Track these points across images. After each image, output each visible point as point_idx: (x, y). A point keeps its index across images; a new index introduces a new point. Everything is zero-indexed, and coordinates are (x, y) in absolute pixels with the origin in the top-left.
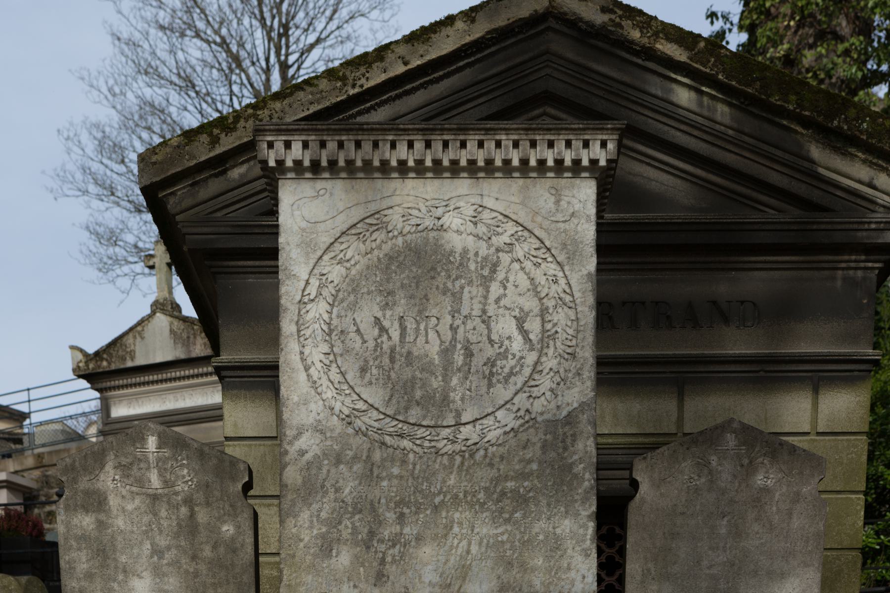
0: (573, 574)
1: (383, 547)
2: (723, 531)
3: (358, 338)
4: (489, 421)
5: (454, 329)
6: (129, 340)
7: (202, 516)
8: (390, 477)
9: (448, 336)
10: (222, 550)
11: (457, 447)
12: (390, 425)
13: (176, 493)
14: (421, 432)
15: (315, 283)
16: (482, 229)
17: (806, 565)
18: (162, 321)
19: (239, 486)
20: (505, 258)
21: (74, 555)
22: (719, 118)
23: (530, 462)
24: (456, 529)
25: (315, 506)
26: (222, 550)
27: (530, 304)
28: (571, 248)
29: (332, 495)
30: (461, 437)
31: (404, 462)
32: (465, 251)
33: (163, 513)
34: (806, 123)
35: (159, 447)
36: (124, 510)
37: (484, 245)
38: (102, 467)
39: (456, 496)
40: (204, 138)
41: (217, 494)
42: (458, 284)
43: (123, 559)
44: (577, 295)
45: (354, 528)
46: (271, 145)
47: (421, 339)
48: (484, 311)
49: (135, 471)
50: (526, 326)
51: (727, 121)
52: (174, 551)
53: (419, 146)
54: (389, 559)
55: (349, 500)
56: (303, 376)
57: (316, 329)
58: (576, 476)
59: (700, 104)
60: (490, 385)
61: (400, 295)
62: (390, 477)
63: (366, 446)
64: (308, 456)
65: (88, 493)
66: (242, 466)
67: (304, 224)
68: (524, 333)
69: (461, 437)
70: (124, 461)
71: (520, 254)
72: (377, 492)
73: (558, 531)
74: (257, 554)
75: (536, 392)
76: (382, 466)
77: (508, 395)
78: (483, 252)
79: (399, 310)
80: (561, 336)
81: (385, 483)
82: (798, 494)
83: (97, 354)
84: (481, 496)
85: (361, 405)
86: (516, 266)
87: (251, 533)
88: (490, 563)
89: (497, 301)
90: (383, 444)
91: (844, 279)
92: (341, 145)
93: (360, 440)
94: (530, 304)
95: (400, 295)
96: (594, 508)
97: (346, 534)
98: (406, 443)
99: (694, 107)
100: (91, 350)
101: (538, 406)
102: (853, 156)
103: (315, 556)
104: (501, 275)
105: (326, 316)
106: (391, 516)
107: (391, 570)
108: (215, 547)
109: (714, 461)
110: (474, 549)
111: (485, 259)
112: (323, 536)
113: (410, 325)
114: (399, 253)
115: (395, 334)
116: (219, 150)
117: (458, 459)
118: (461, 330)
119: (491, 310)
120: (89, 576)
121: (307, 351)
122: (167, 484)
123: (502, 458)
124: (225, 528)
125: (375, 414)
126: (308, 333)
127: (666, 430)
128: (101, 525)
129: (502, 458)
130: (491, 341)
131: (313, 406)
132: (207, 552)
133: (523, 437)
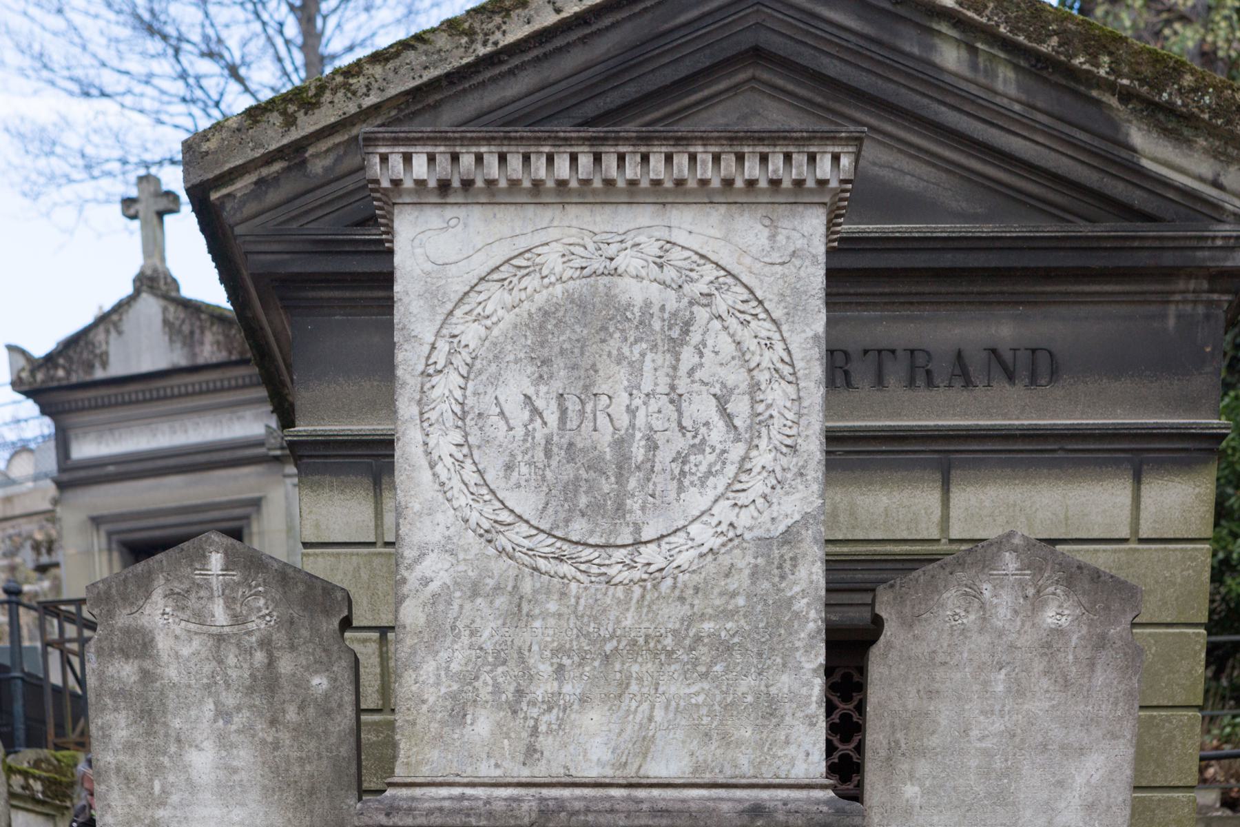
0: (792, 750)
1: (534, 712)
2: (1000, 688)
3: (502, 425)
4: (679, 539)
5: (632, 411)
6: (99, 336)
7: (285, 665)
8: (545, 615)
9: (623, 420)
10: (311, 711)
11: (637, 574)
12: (543, 544)
13: (249, 633)
14: (587, 553)
15: (443, 346)
16: (670, 274)
17: (1115, 736)
18: (150, 306)
19: (336, 623)
20: (702, 314)
21: (109, 717)
22: (1000, 87)
23: (734, 595)
24: (634, 688)
25: (443, 655)
26: (311, 711)
27: (736, 377)
28: (794, 297)
29: (465, 640)
30: (641, 560)
31: (563, 595)
32: (648, 304)
33: (231, 660)
34: (1126, 96)
35: (226, 568)
36: (177, 656)
37: (672, 295)
38: (148, 596)
39: (634, 643)
40: (276, 118)
41: (305, 633)
42: (637, 349)
43: (176, 723)
44: (799, 365)
45: (496, 685)
46: (384, 159)
47: (587, 425)
48: (673, 388)
49: (192, 602)
50: (730, 408)
51: (1012, 91)
52: (246, 713)
53: (585, 161)
54: (543, 728)
55: (489, 646)
56: (426, 475)
57: (444, 410)
58: (797, 615)
59: (974, 67)
60: (681, 489)
61: (559, 363)
62: (545, 615)
63: (512, 573)
64: (434, 587)
65: (128, 632)
66: (339, 595)
67: (428, 267)
68: (728, 417)
69: (641, 560)
70: (178, 587)
71: (722, 309)
72: (527, 636)
73: (773, 690)
74: (359, 711)
75: (743, 499)
76: (533, 601)
77: (704, 502)
78: (672, 305)
79: (557, 386)
80: (777, 422)
81: (537, 624)
82: (1103, 637)
83: (50, 359)
84: (669, 642)
85: (505, 516)
86: (716, 324)
87: (352, 688)
88: (680, 734)
89: (691, 372)
90: (536, 569)
91: (1179, 317)
92: (479, 159)
93: (505, 562)
94: (736, 377)
95: (559, 363)
96: (822, 659)
97: (485, 693)
98: (565, 569)
99: (965, 71)
100: (39, 350)
101: (744, 519)
102: (1189, 143)
103: (443, 723)
104: (695, 338)
105: (458, 394)
106: (545, 669)
107: (545, 742)
108: (301, 708)
109: (987, 590)
110: (659, 714)
111: (674, 315)
112: (454, 697)
113: (572, 405)
114: (557, 306)
115: (552, 418)
116: (294, 135)
117: (637, 591)
118: (641, 414)
119: (683, 385)
120: (131, 747)
121: (432, 442)
122: (237, 620)
123: (697, 590)
124: (316, 681)
125: (524, 529)
126: (433, 416)
127: (924, 535)
128: (147, 677)
129: (697, 590)
130: (682, 428)
131: (440, 517)
132: (292, 715)
133: (725, 560)
